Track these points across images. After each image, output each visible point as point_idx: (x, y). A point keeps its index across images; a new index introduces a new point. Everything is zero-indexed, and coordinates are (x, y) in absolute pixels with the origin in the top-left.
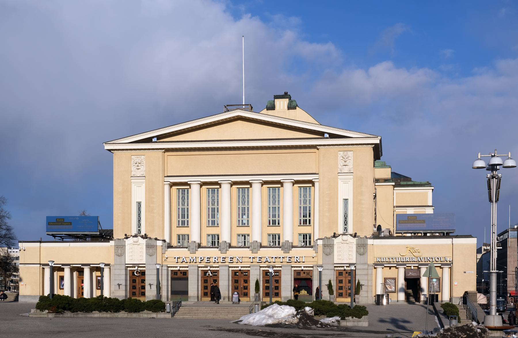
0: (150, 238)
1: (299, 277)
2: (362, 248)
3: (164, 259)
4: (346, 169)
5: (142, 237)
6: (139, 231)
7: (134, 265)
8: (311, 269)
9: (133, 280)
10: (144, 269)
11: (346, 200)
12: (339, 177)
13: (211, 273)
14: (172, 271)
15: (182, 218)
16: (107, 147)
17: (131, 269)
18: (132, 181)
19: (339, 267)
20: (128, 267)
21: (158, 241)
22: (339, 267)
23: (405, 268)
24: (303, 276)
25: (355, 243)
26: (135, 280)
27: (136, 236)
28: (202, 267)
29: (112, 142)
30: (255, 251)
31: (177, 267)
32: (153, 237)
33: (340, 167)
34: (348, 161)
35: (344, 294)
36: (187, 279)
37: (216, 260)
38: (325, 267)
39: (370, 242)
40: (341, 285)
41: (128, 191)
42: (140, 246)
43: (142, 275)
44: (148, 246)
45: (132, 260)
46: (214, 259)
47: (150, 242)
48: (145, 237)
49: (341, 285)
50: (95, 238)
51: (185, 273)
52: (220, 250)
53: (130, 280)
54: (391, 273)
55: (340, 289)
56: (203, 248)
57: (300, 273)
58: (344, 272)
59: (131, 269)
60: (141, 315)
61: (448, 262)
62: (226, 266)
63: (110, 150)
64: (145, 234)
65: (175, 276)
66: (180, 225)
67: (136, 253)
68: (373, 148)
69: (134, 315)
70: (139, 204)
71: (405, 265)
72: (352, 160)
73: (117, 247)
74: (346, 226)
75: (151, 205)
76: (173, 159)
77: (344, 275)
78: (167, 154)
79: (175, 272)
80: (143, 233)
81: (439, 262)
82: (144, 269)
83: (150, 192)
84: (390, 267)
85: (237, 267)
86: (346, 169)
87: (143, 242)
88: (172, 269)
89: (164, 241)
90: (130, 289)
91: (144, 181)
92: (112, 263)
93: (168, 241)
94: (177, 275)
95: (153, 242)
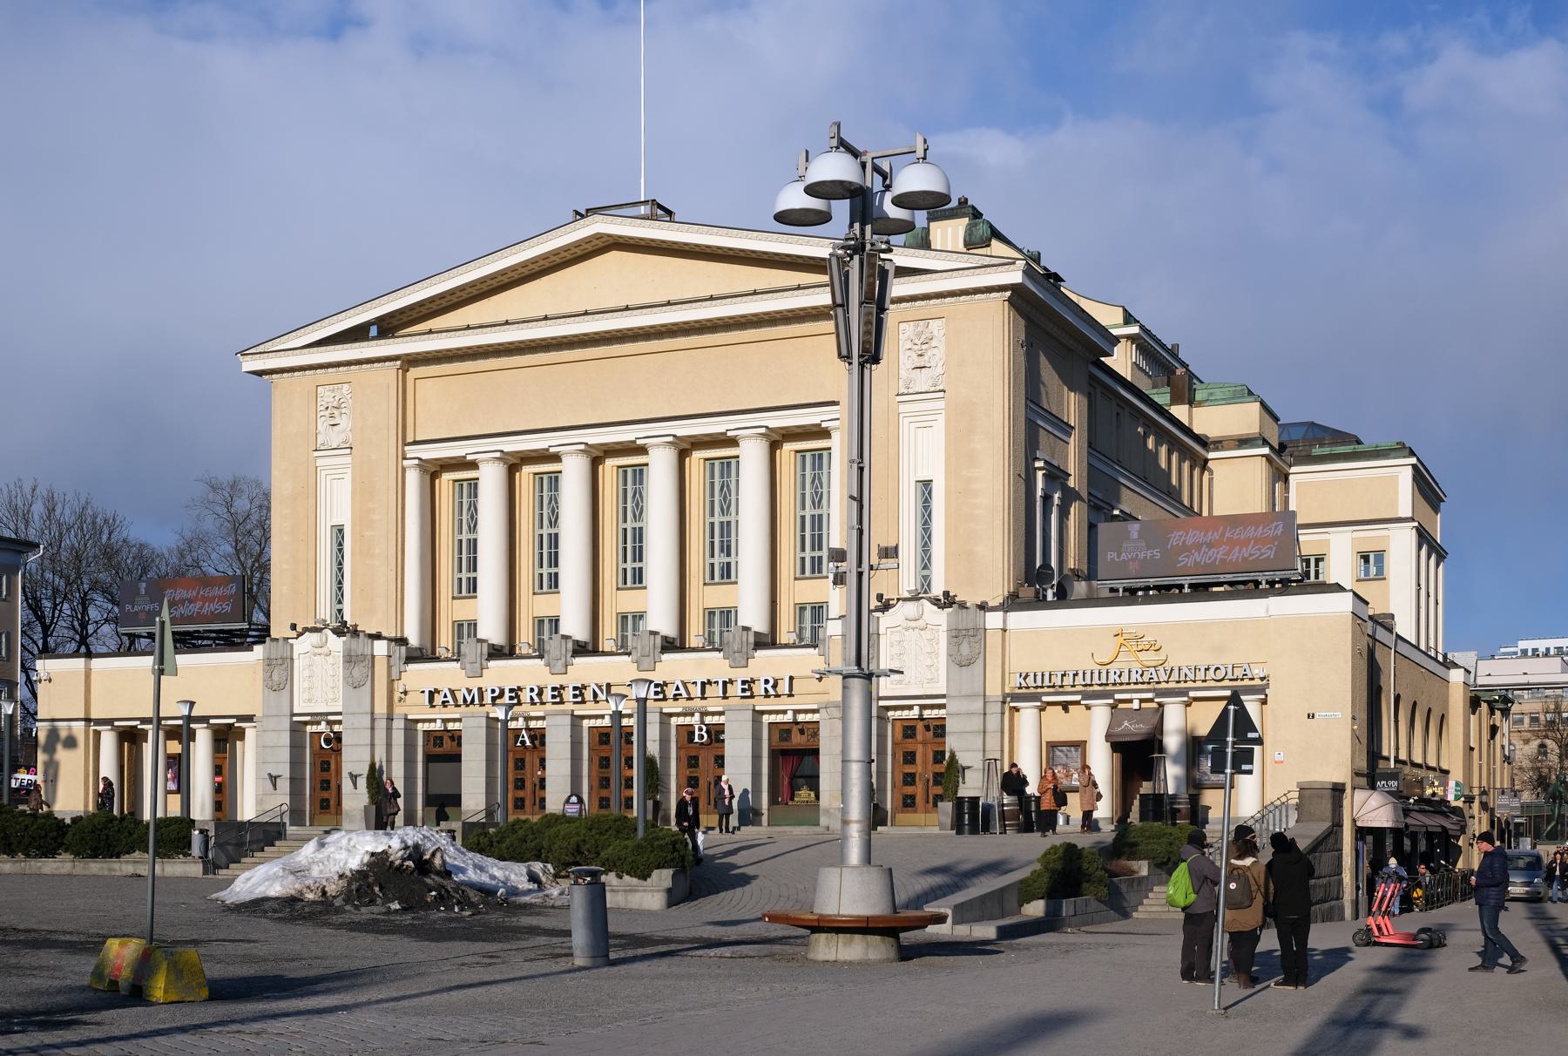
0: (963, 605)
1: (785, 745)
2: (967, 643)
3: (397, 696)
4: (922, 381)
5: (936, 602)
6: (926, 582)
7: (316, 718)
8: (816, 717)
9: (323, 763)
10: (942, 713)
11: (927, 484)
12: (902, 408)
13: (530, 737)
14: (426, 733)
15: (813, 549)
16: (250, 364)
17: (681, 721)
18: (319, 462)
19: (902, 708)
20: (888, 708)
21: (376, 643)
22: (902, 708)
23: (1114, 707)
24: (797, 740)
25: (944, 627)
26: (913, 754)
27: (915, 598)
28: (678, 715)
29: (268, 347)
30: (647, 662)
31: (434, 721)
32: (972, 600)
33: (903, 374)
34: (929, 353)
35: (919, 800)
36: (457, 758)
37: (769, 687)
38: (953, 706)
39: (994, 620)
40: (909, 769)
41: (310, 493)
42: (927, 634)
43: (936, 735)
44: (350, 659)
45: (310, 700)
46: (763, 686)
47: (967, 619)
48: (947, 601)
49: (909, 769)
50: (1285, 587)
51: (456, 737)
52: (548, 665)
53: (591, 760)
54: (1061, 726)
55: (906, 783)
56: (604, 654)
57: (789, 731)
58: (920, 726)
59: (681, 721)
60: (117, 866)
61: (1257, 682)
62: (563, 713)
63: (260, 373)
64: (946, 594)
65: (438, 750)
66: (464, 593)
67: (319, 680)
68: (1010, 300)
69: (96, 867)
70: (927, 484)
71: (1109, 695)
72: (942, 348)
73: (269, 662)
74: (925, 572)
75: (367, 534)
76: (429, 386)
77: (919, 737)
78: (414, 372)
79: (601, 735)
80: (937, 590)
81: (1226, 683)
82: (942, 713)
83: (362, 492)
84: (1065, 706)
85: (430, 721)
86: (922, 381)
87: (336, 644)
88: (593, 723)
89: (402, 641)
90: (591, 788)
91: (348, 459)
92: (259, 714)
93: (414, 641)
94: (441, 745)
95: (360, 645)
